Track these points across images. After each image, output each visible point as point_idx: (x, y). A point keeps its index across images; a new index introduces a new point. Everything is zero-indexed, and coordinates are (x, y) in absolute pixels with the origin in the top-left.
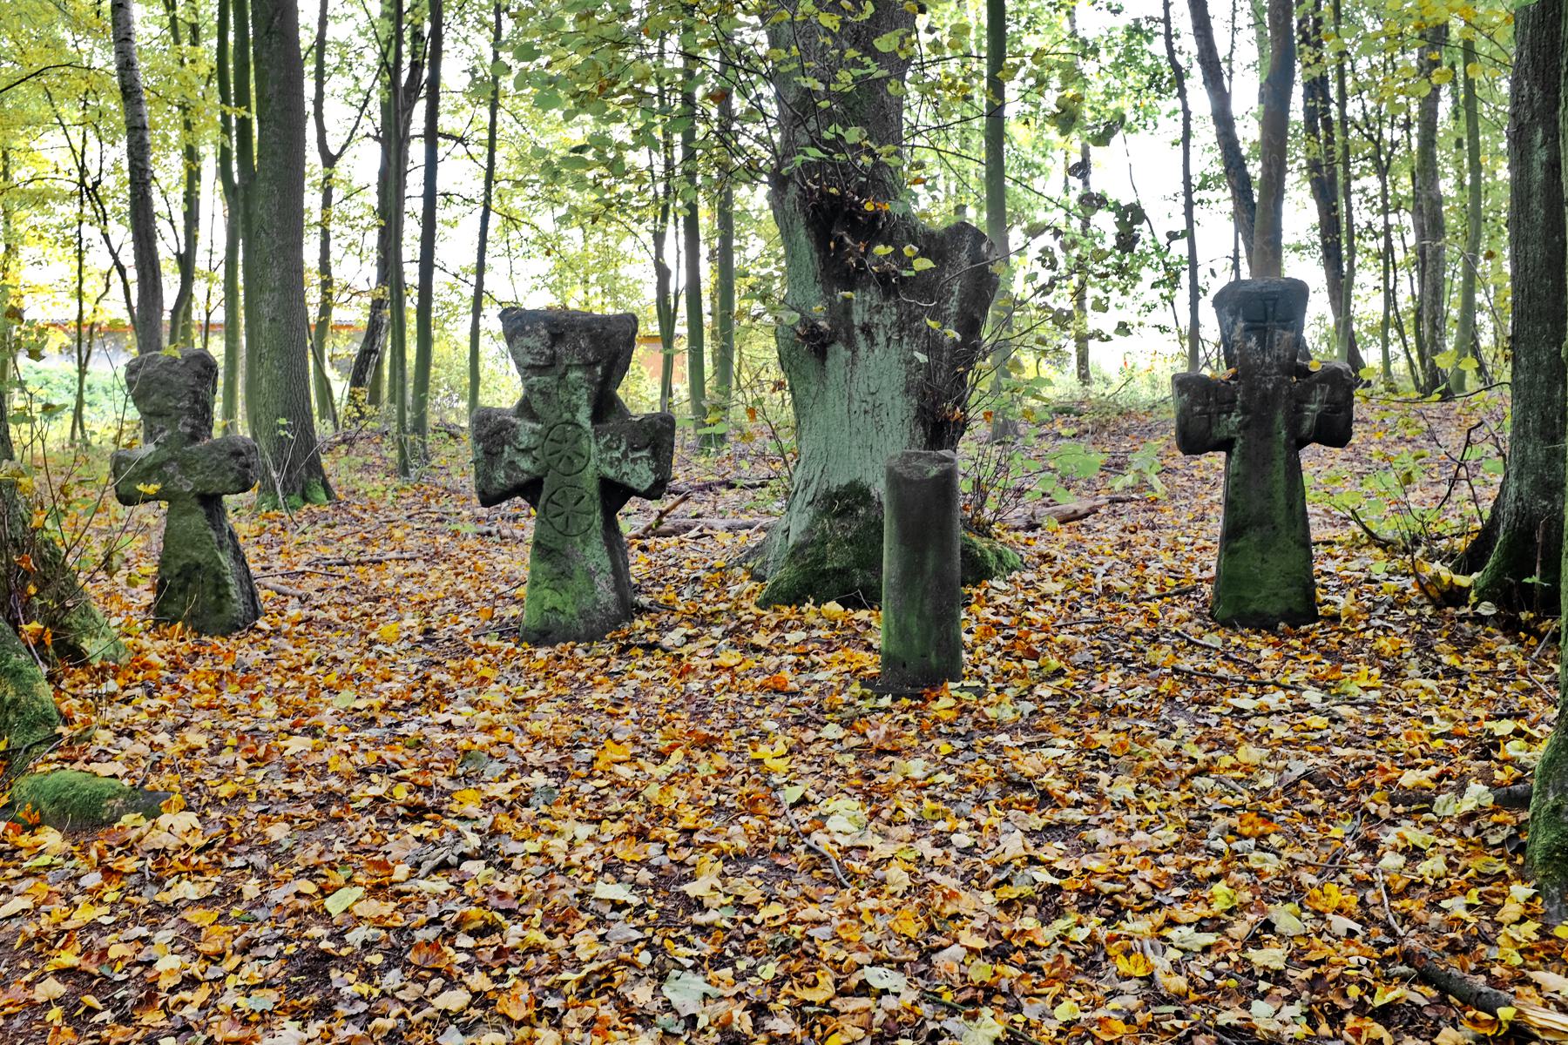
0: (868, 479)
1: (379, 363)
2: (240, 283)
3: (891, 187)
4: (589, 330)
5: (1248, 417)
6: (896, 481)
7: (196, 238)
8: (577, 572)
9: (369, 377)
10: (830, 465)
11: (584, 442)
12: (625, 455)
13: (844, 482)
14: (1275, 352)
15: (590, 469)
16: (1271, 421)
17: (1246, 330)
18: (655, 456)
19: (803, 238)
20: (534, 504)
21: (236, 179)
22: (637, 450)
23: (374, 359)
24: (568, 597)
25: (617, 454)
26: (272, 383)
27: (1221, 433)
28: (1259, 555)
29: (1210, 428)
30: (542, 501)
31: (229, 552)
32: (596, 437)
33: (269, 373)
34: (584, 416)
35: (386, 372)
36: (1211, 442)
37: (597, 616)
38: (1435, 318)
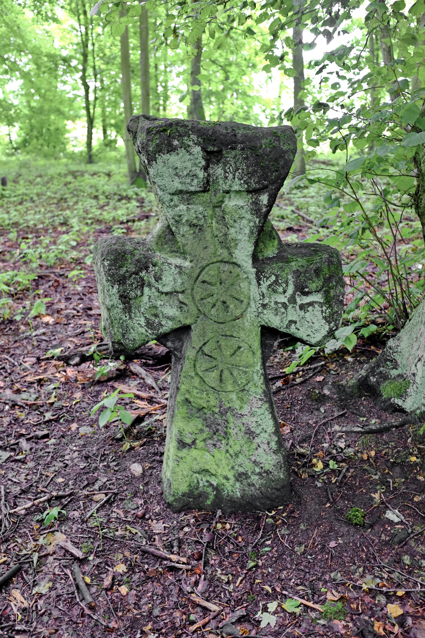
4: (253, 149)
12: (292, 300)
15: (250, 314)
18: (328, 301)
22: (306, 294)
24: (220, 455)
25: (282, 299)
32: (258, 279)
37: (255, 479)
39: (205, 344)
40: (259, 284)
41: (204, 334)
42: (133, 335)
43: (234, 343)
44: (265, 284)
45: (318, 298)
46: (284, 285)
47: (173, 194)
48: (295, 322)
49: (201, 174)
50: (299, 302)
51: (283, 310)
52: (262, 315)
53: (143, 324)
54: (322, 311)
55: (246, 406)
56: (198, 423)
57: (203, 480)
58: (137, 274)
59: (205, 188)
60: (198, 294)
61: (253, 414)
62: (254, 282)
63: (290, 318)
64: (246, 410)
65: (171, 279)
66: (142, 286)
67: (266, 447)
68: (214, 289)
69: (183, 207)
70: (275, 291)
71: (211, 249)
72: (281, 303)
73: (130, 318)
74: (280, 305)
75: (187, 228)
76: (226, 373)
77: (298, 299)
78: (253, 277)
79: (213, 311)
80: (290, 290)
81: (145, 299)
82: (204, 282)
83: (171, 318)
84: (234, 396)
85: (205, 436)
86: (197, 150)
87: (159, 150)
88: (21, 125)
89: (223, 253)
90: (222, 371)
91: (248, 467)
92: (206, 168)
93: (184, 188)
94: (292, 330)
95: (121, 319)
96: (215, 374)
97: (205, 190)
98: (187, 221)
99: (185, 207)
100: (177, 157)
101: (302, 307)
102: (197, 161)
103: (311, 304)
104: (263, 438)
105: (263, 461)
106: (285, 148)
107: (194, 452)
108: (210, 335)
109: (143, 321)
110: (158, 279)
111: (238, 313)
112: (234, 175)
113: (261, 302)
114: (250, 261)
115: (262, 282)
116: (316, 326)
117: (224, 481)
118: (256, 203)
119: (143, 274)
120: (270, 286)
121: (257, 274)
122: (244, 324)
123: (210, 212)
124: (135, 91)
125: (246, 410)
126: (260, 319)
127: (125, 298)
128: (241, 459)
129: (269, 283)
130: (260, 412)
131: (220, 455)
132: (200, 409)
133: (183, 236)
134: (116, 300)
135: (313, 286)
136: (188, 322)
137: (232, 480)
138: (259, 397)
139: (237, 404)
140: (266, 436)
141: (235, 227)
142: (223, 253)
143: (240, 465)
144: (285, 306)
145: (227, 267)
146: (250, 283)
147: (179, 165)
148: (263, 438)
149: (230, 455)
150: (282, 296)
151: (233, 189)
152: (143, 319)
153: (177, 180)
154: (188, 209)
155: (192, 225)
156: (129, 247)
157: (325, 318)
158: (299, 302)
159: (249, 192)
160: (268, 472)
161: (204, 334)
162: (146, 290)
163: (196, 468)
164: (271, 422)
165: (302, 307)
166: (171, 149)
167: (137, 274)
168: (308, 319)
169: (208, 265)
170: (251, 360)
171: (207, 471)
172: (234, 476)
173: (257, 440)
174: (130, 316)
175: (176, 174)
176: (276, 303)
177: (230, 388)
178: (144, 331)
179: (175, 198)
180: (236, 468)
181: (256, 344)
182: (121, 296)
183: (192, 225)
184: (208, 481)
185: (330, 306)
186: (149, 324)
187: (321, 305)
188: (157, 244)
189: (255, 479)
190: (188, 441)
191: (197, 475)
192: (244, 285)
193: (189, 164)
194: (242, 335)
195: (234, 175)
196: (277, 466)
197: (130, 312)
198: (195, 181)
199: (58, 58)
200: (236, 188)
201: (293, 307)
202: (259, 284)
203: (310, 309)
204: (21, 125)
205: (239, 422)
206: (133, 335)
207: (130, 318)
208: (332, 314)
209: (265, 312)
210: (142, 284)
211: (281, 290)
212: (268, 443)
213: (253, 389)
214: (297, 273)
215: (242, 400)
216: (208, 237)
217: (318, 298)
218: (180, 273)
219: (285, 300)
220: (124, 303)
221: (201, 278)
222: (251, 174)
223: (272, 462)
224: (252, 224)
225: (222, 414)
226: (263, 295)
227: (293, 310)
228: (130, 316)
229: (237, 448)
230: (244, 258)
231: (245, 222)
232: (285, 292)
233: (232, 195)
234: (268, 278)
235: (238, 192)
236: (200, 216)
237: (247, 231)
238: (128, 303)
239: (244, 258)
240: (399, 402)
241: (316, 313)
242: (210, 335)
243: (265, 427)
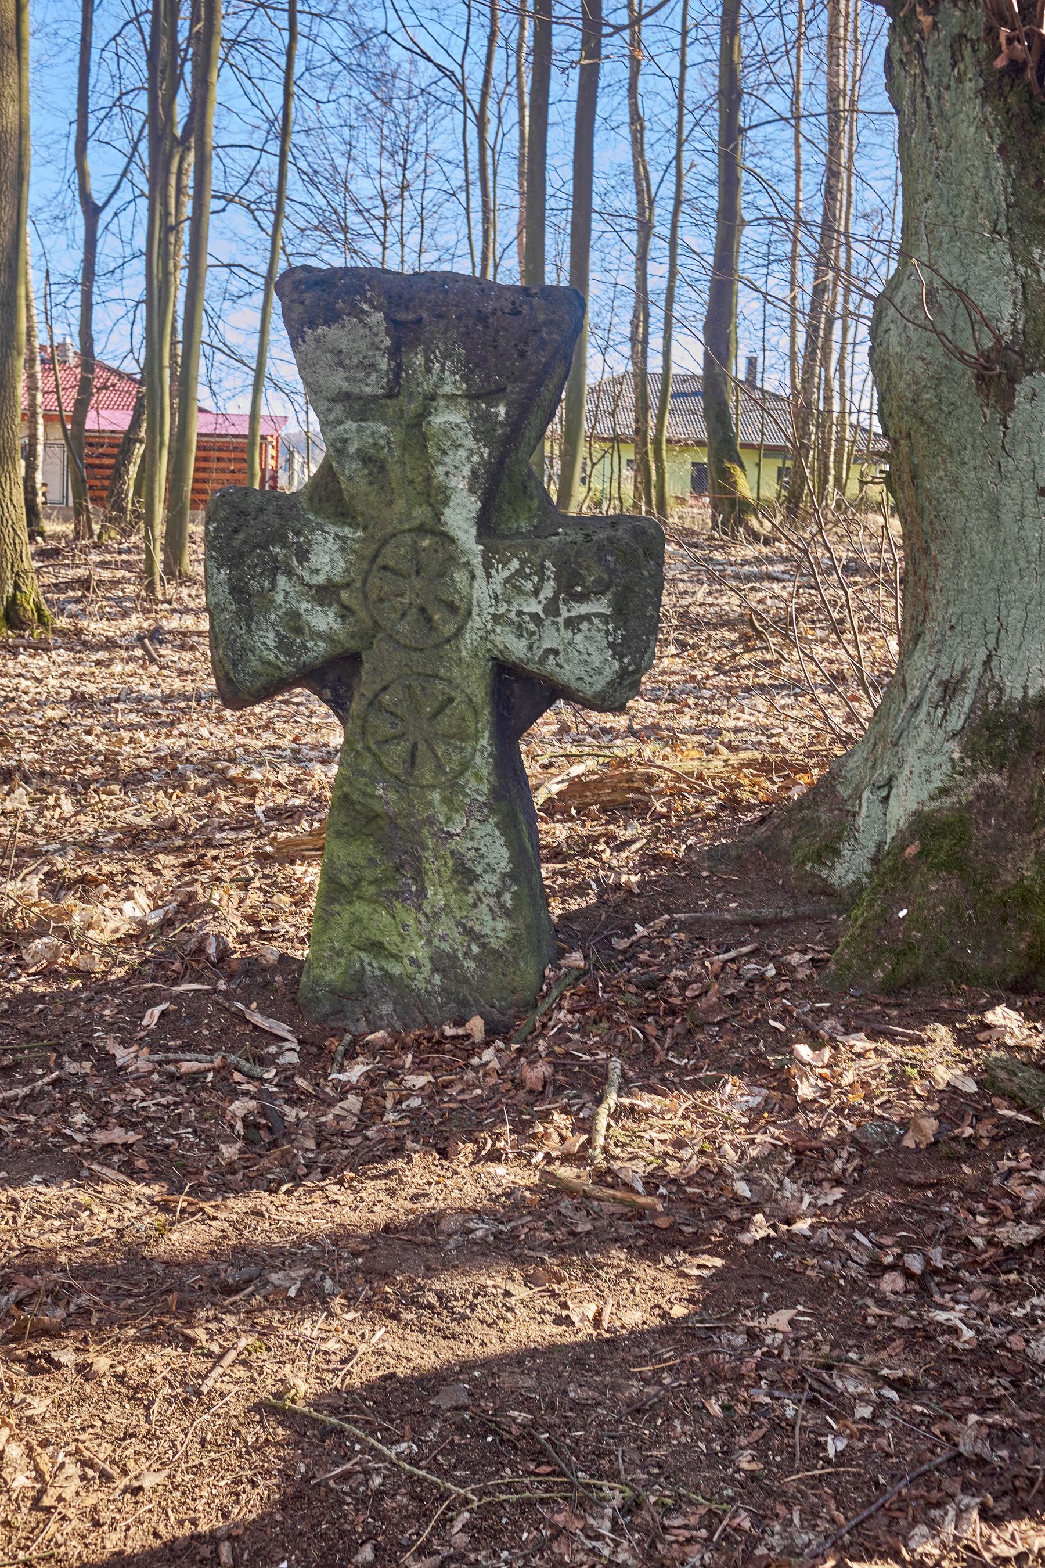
12: (551, 607)
25: (534, 607)
32: (487, 566)
39: (385, 688)
40: (489, 576)
44: (500, 575)
46: (536, 579)
47: (334, 400)
48: (556, 652)
50: (565, 614)
51: (532, 627)
52: (492, 636)
53: (272, 644)
54: (607, 633)
55: (457, 817)
58: (265, 547)
59: (391, 389)
62: (479, 572)
63: (547, 645)
65: (327, 559)
67: (492, 901)
69: (351, 425)
70: (519, 590)
72: (530, 614)
73: (249, 631)
74: (527, 618)
75: (356, 465)
76: (422, 747)
77: (563, 609)
78: (477, 561)
79: (403, 627)
80: (548, 591)
82: (385, 568)
88: (335, 1067)
90: (415, 746)
92: (394, 353)
95: (231, 632)
98: (359, 450)
99: (354, 425)
100: (341, 333)
102: (377, 340)
103: (587, 618)
104: (489, 882)
105: (487, 931)
109: (271, 639)
110: (303, 555)
112: (443, 365)
113: (492, 610)
114: (474, 531)
115: (493, 572)
117: (412, 969)
120: (507, 580)
121: (484, 555)
122: (459, 650)
124: (887, 331)
126: (489, 646)
127: (241, 592)
129: (507, 573)
133: (350, 478)
137: (427, 967)
138: (482, 799)
140: (495, 879)
141: (445, 464)
143: (443, 938)
146: (473, 577)
147: (344, 345)
148: (489, 882)
149: (425, 914)
150: (533, 601)
151: (440, 392)
152: (271, 635)
153: (342, 374)
154: (360, 430)
157: (611, 645)
158: (565, 614)
165: (570, 623)
166: (332, 318)
167: (265, 547)
168: (581, 647)
169: (394, 535)
172: (431, 959)
174: (249, 626)
175: (340, 364)
176: (520, 613)
177: (428, 778)
178: (272, 657)
179: (339, 407)
180: (436, 942)
182: (233, 590)
184: (381, 969)
187: (605, 618)
188: (311, 499)
191: (363, 955)
192: (460, 577)
193: (363, 345)
195: (443, 365)
197: (250, 619)
198: (374, 377)
201: (553, 623)
202: (489, 576)
203: (584, 626)
204: (335, 1067)
207: (249, 631)
209: (498, 629)
211: (529, 586)
212: (498, 895)
213: (473, 783)
218: (342, 549)
219: (539, 609)
220: (238, 602)
221: (380, 561)
223: (503, 935)
224: (476, 459)
226: (496, 598)
227: (553, 629)
228: (249, 626)
230: (461, 524)
231: (462, 453)
232: (536, 593)
233: (442, 402)
234: (504, 565)
235: (451, 398)
236: (382, 442)
237: (466, 471)
238: (247, 601)
239: (461, 524)
241: (594, 633)
243: (493, 862)
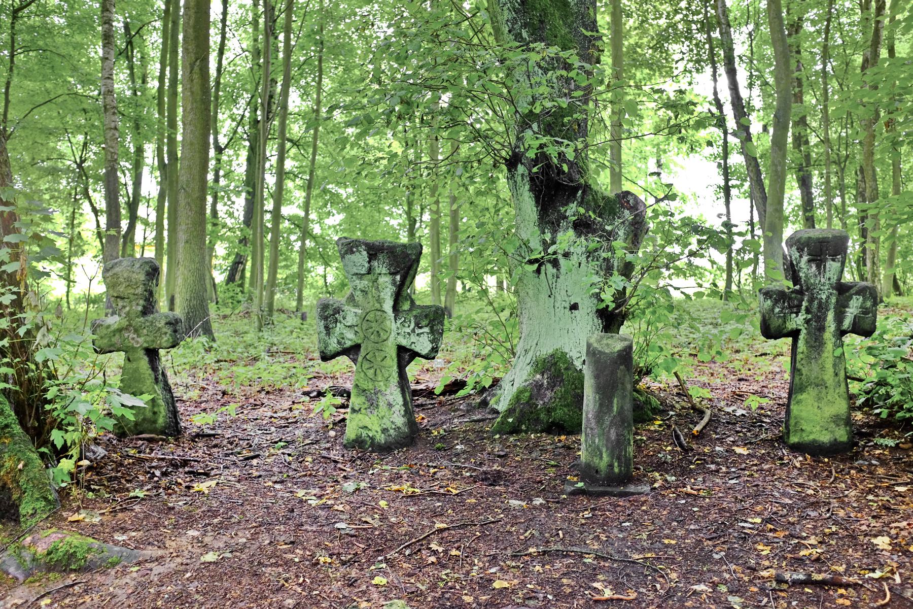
0: (573, 354)
1: (244, 270)
2: (166, 222)
3: (582, 168)
4: (392, 252)
5: (809, 316)
6: (591, 352)
7: (731, 89)
8: (381, 404)
9: (237, 277)
10: (542, 340)
11: (388, 323)
12: (413, 331)
13: (550, 351)
14: (827, 275)
15: (391, 339)
16: (825, 319)
17: (809, 261)
18: (432, 332)
19: (527, 198)
20: (355, 361)
21: (166, 162)
22: (421, 328)
23: (241, 267)
24: (374, 418)
25: (408, 330)
26: (185, 280)
27: (791, 325)
28: (816, 404)
29: (785, 322)
30: (360, 359)
31: (162, 385)
32: (396, 319)
33: (183, 274)
34: (388, 305)
35: (248, 274)
36: (785, 331)
37: (392, 432)
38: (874, 258)
41: (367, 349)
42: (330, 348)
43: (383, 354)
44: (399, 322)
45: (427, 330)
49: (367, 265)
56: (363, 399)
57: (364, 433)
60: (365, 326)
61: (392, 394)
64: (388, 392)
66: (336, 322)
68: (373, 325)
69: (358, 282)
71: (371, 304)
76: (378, 371)
78: (393, 318)
80: (412, 325)
81: (337, 329)
83: (351, 340)
84: (382, 384)
85: (366, 406)
86: (365, 253)
87: (346, 253)
89: (377, 306)
91: (388, 425)
92: (369, 262)
93: (358, 272)
94: (413, 347)
96: (372, 371)
97: (369, 273)
101: (418, 335)
106: (409, 252)
107: (360, 416)
108: (370, 349)
109: (336, 341)
110: (344, 318)
111: (385, 337)
116: (425, 345)
118: (394, 280)
119: (337, 316)
123: (371, 284)
125: (388, 392)
128: (385, 420)
130: (395, 393)
131: (374, 418)
132: (364, 391)
134: (322, 329)
135: (424, 323)
136: (359, 342)
137: (380, 432)
139: (383, 388)
142: (377, 306)
144: (409, 334)
145: (379, 313)
155: (362, 291)
156: (331, 302)
159: (390, 274)
160: (399, 428)
161: (367, 349)
162: (338, 324)
163: (361, 425)
164: (401, 399)
165: (418, 335)
166: (352, 252)
170: (391, 364)
171: (366, 427)
173: (393, 409)
181: (394, 355)
183: (362, 291)
185: (433, 335)
186: (339, 343)
187: (428, 333)
189: (392, 432)
190: (357, 409)
194: (387, 349)
196: (404, 424)
199: (335, 212)
200: (384, 272)
205: (384, 399)
206: (330, 348)
208: (434, 339)
210: (336, 321)
214: (415, 317)
215: (386, 385)
216: (370, 296)
217: (427, 330)
222: (391, 265)
225: (376, 394)
229: (383, 414)
240: (496, 407)
242: (370, 349)
